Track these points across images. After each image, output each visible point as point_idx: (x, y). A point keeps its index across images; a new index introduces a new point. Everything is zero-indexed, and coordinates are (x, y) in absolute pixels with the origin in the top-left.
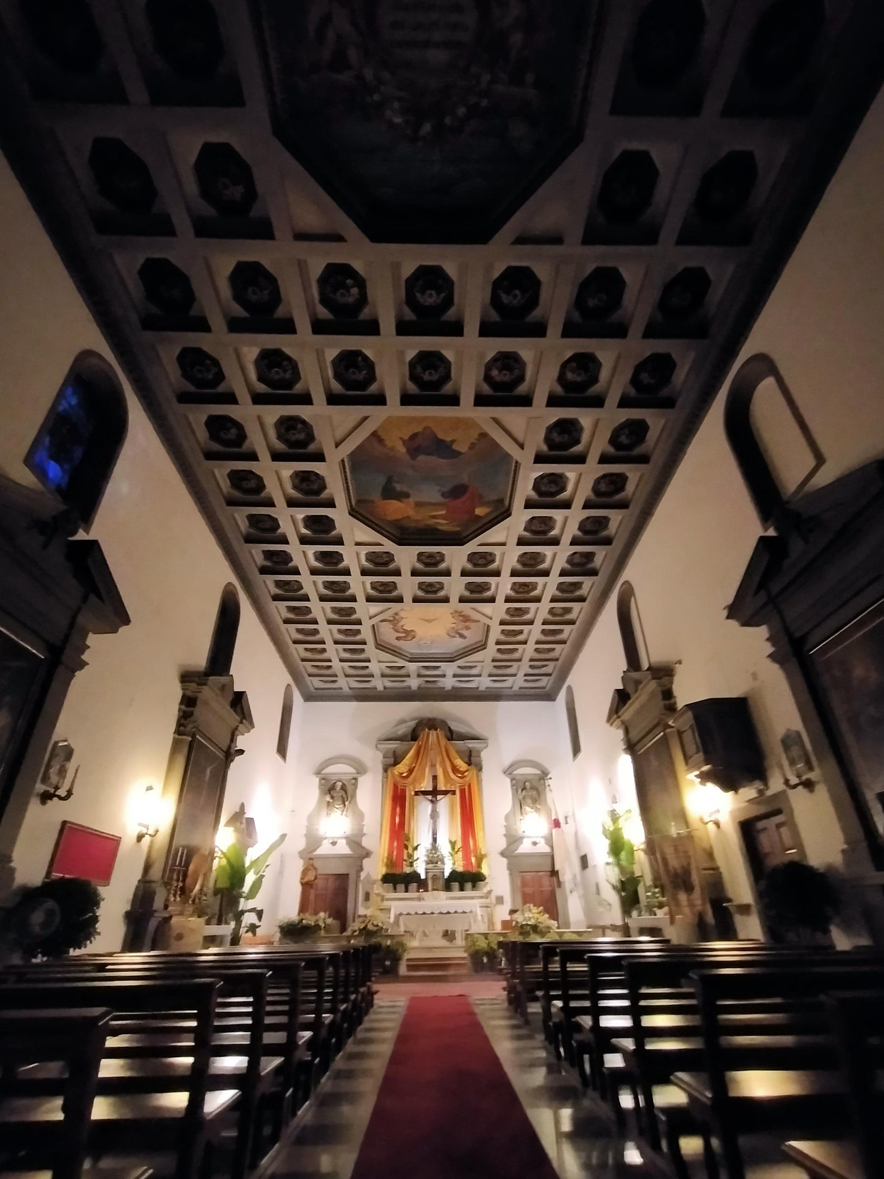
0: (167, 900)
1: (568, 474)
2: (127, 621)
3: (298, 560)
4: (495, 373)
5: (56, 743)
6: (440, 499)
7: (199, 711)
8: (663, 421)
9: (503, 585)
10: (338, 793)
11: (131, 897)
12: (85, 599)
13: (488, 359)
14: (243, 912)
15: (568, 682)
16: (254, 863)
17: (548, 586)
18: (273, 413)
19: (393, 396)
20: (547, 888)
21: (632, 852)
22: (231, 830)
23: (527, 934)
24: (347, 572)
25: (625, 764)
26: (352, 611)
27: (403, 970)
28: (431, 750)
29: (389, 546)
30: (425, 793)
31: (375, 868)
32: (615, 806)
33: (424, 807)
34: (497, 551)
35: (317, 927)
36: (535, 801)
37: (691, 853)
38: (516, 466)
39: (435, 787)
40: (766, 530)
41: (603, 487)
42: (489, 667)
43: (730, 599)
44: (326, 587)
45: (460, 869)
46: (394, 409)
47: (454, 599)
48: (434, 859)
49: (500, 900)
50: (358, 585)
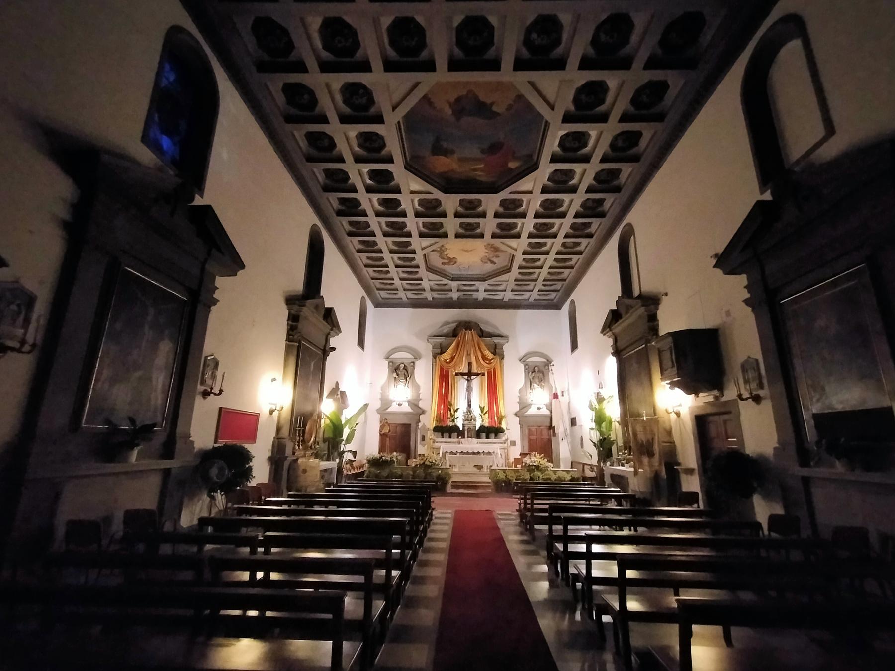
0: (294, 448)
1: (591, 132)
2: (243, 267)
3: (365, 205)
4: (534, 36)
5: (206, 357)
6: (479, 155)
7: (302, 325)
8: (682, 82)
9: (528, 224)
10: (401, 371)
11: (270, 448)
12: (209, 254)
13: (528, 23)
14: (343, 452)
15: (573, 296)
16: (348, 421)
17: (563, 226)
18: (338, 80)
19: (441, 62)
20: (546, 436)
21: (610, 423)
22: (330, 400)
23: (533, 471)
24: (409, 235)
25: (611, 364)
26: (408, 244)
27: (449, 489)
28: (466, 344)
29: (437, 194)
30: (463, 374)
31: (428, 421)
32: (600, 390)
33: (462, 384)
34: (525, 198)
35: (392, 461)
36: (541, 381)
37: (656, 431)
38: (546, 126)
39: (470, 370)
40: (762, 192)
41: (620, 143)
42: (512, 285)
43: (720, 250)
44: (387, 226)
45: (486, 425)
46: (442, 75)
47: (488, 235)
48: (469, 417)
49: (513, 443)
50: (413, 224)
